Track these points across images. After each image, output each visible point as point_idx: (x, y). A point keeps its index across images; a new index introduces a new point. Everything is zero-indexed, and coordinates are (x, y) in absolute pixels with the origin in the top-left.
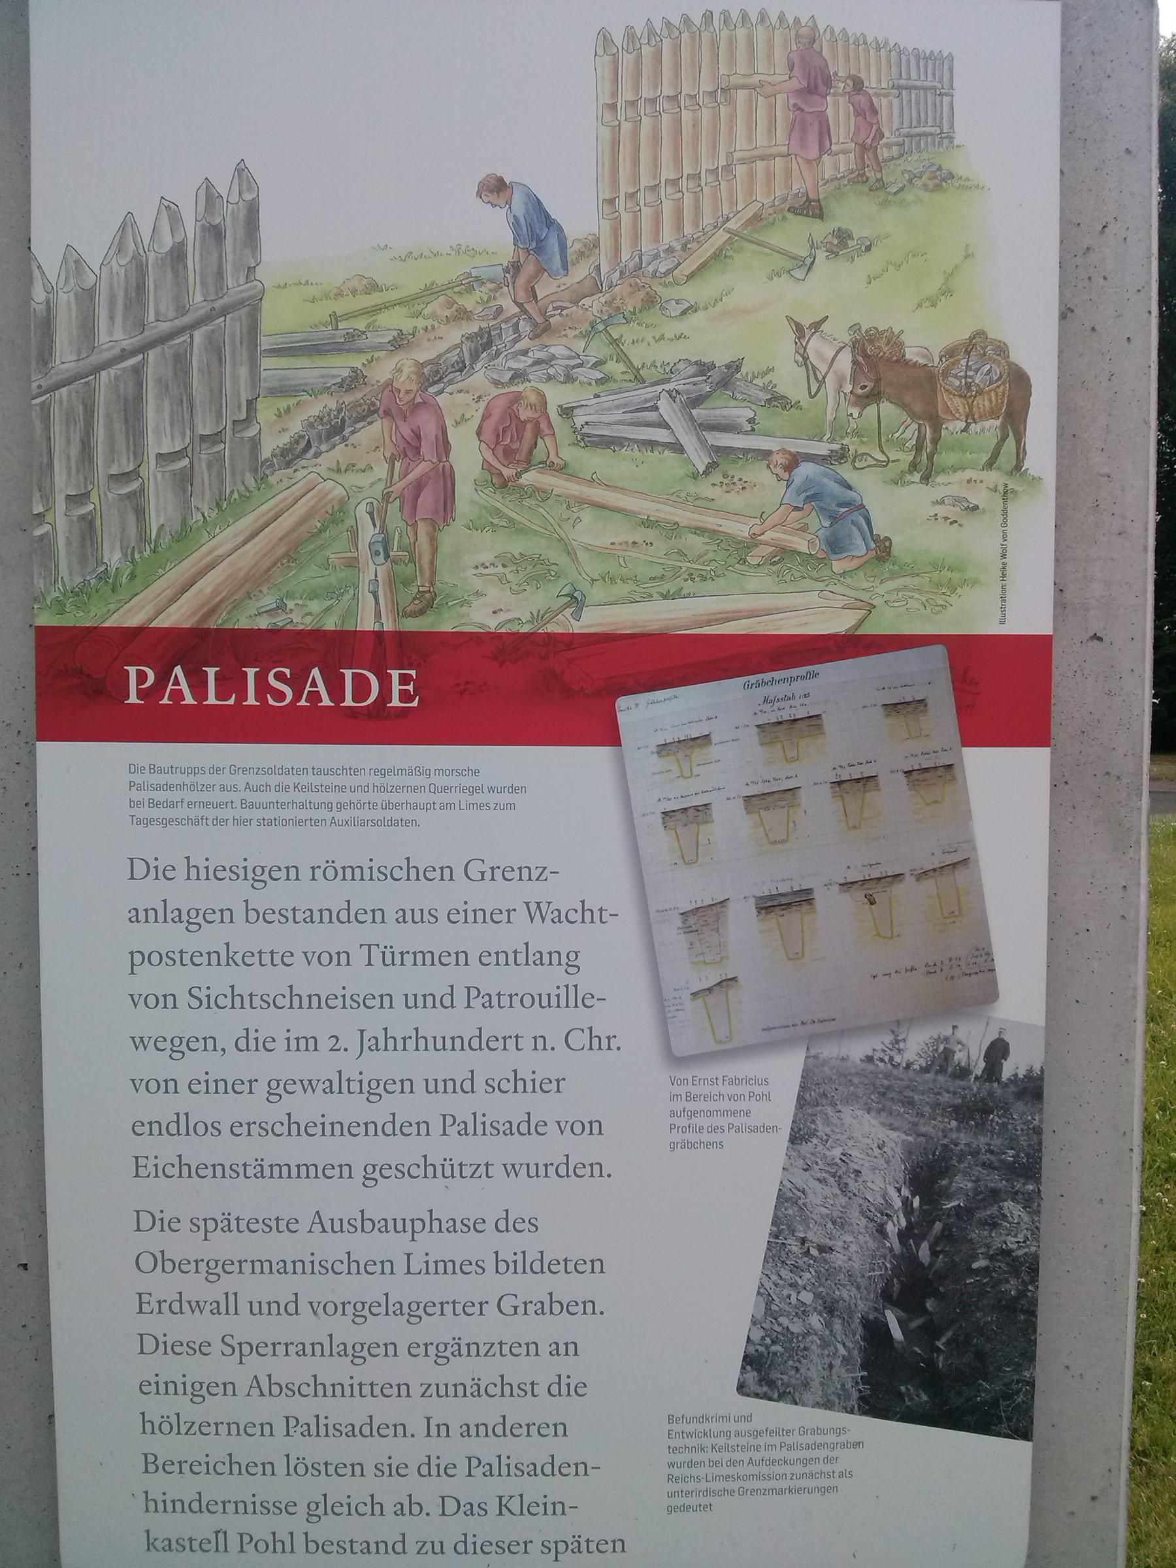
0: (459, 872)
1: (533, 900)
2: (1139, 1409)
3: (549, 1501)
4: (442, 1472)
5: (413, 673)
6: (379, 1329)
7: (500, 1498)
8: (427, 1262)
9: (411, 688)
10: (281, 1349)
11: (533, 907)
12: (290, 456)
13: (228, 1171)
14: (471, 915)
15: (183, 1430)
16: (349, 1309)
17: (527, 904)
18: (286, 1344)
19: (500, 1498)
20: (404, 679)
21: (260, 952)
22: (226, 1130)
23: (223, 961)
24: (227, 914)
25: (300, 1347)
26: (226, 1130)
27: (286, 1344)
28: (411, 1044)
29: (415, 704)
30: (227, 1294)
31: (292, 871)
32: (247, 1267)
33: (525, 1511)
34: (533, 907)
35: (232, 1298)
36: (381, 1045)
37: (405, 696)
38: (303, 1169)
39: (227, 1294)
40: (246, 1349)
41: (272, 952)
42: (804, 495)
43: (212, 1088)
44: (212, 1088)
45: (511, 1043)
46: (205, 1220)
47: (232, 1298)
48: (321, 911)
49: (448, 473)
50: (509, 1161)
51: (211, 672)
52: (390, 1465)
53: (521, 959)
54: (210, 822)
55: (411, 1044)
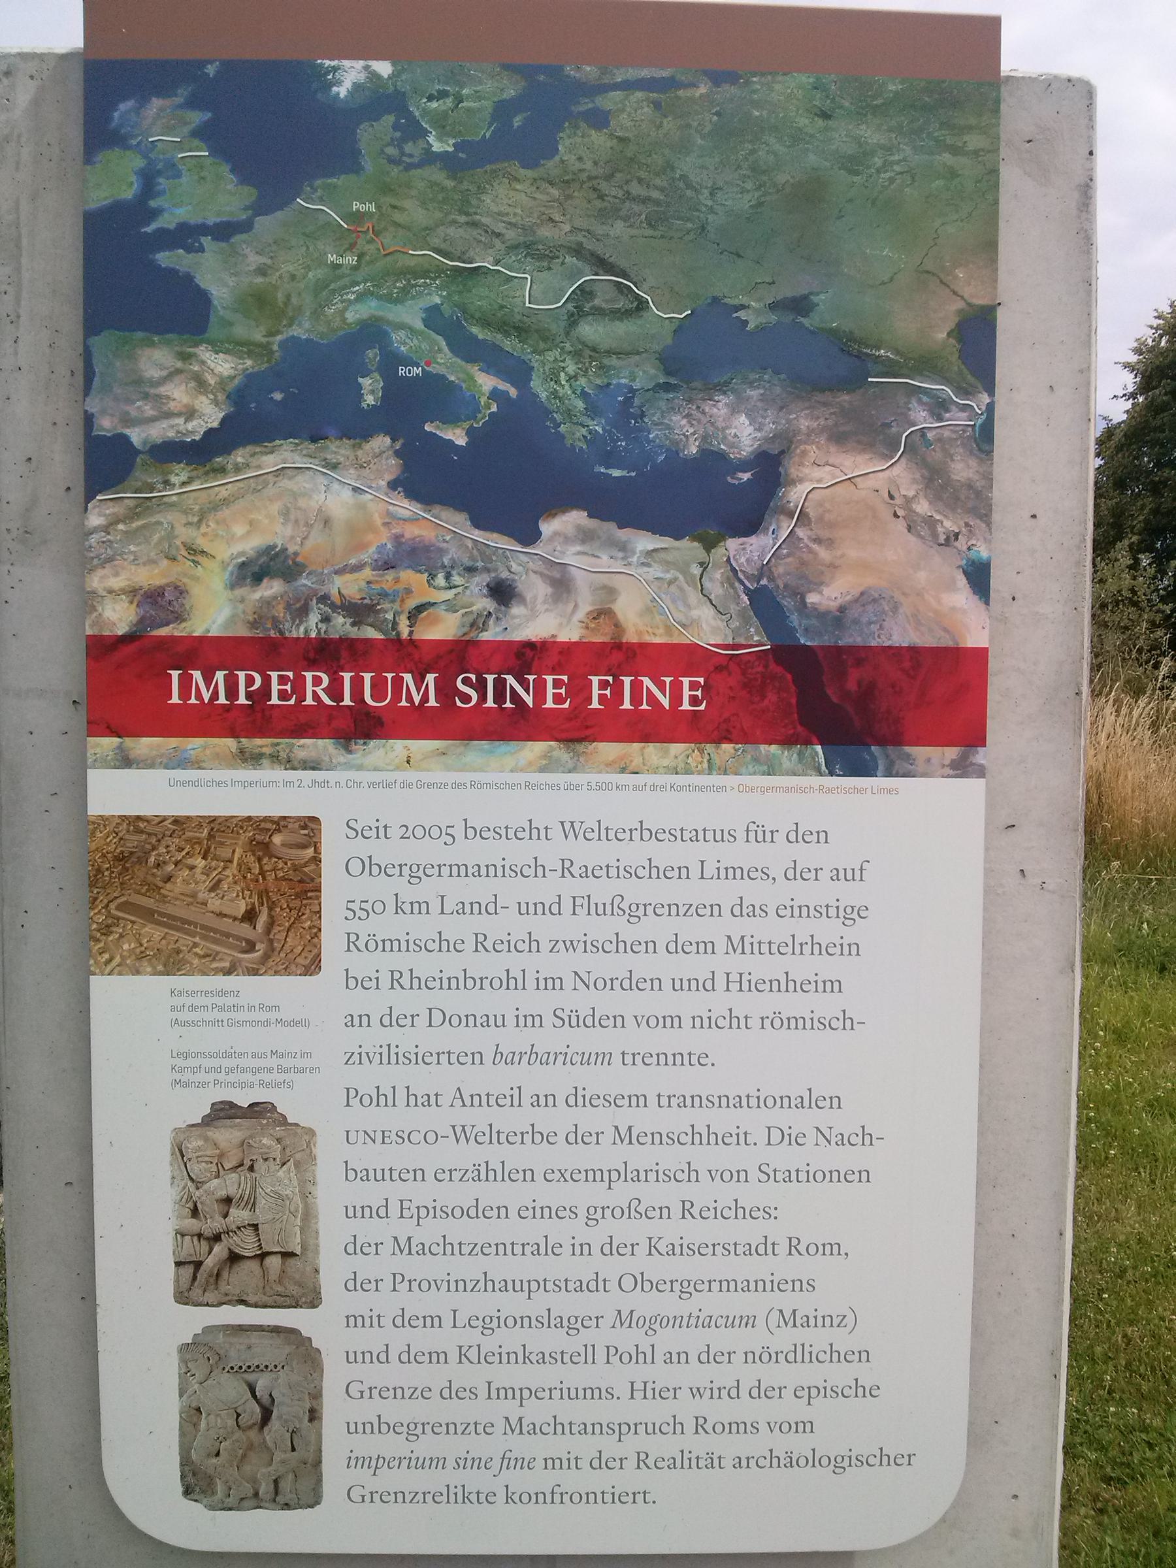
7: (460, 1347)
14: (505, 1357)
19: (460, 1347)
21: (608, 866)
22: (772, 911)
23: (521, 1359)
26: (772, 911)
30: (586, 1346)
31: (684, 871)
33: (482, 1360)
35: (590, 1349)
38: (589, 1392)
39: (586, 1346)
41: (770, 943)
43: (446, 985)
44: (446, 985)
45: (640, 1498)
47: (590, 1349)
49: (588, 732)
54: (225, 1023)
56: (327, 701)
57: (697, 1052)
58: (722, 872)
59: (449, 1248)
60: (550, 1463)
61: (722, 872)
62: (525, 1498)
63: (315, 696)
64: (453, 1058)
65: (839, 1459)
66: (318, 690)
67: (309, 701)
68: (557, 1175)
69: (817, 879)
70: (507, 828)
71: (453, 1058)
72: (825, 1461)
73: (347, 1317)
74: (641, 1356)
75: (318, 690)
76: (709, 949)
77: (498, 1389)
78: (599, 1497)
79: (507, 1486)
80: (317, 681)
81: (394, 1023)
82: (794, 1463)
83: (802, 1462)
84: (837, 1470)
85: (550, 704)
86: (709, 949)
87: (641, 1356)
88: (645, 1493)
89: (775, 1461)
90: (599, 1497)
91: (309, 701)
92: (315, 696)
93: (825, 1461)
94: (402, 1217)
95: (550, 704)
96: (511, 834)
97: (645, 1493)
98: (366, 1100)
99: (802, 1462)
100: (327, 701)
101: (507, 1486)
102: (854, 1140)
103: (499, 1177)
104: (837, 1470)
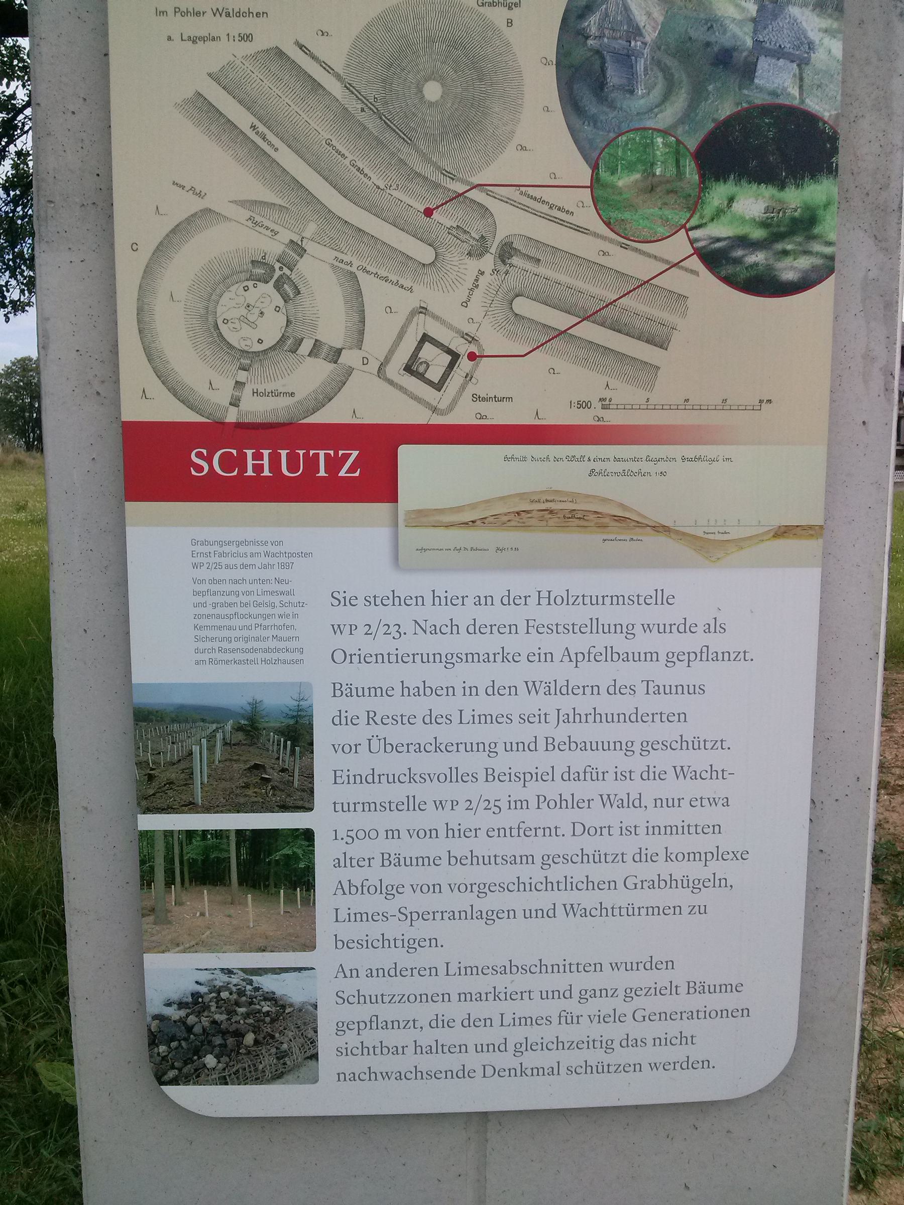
0: (620, 885)
1: (568, 902)
2: (309, 776)
3: (542, 652)
4: (649, 859)
10: (438, 916)
15: (571, 601)
16: (475, 888)
18: (442, 912)
25: (451, 913)
27: (442, 912)
28: (591, 718)
36: (571, 719)
40: (415, 916)
42: (593, 108)
43: (543, 659)
44: (543, 659)
48: (486, 597)
51: (322, 473)
53: (562, 886)
55: (591, 718)
58: (477, 718)
61: (477, 718)
62: (680, 857)
64: (664, 718)
68: (732, 855)
69: (434, 919)
71: (664, 718)
74: (564, 803)
76: (525, 806)
77: (700, 860)
79: (666, 848)
81: (570, 692)
86: (525, 806)
87: (564, 803)
88: (609, 827)
94: (335, 783)
96: (378, 601)
97: (609, 827)
101: (666, 848)
103: (570, 805)
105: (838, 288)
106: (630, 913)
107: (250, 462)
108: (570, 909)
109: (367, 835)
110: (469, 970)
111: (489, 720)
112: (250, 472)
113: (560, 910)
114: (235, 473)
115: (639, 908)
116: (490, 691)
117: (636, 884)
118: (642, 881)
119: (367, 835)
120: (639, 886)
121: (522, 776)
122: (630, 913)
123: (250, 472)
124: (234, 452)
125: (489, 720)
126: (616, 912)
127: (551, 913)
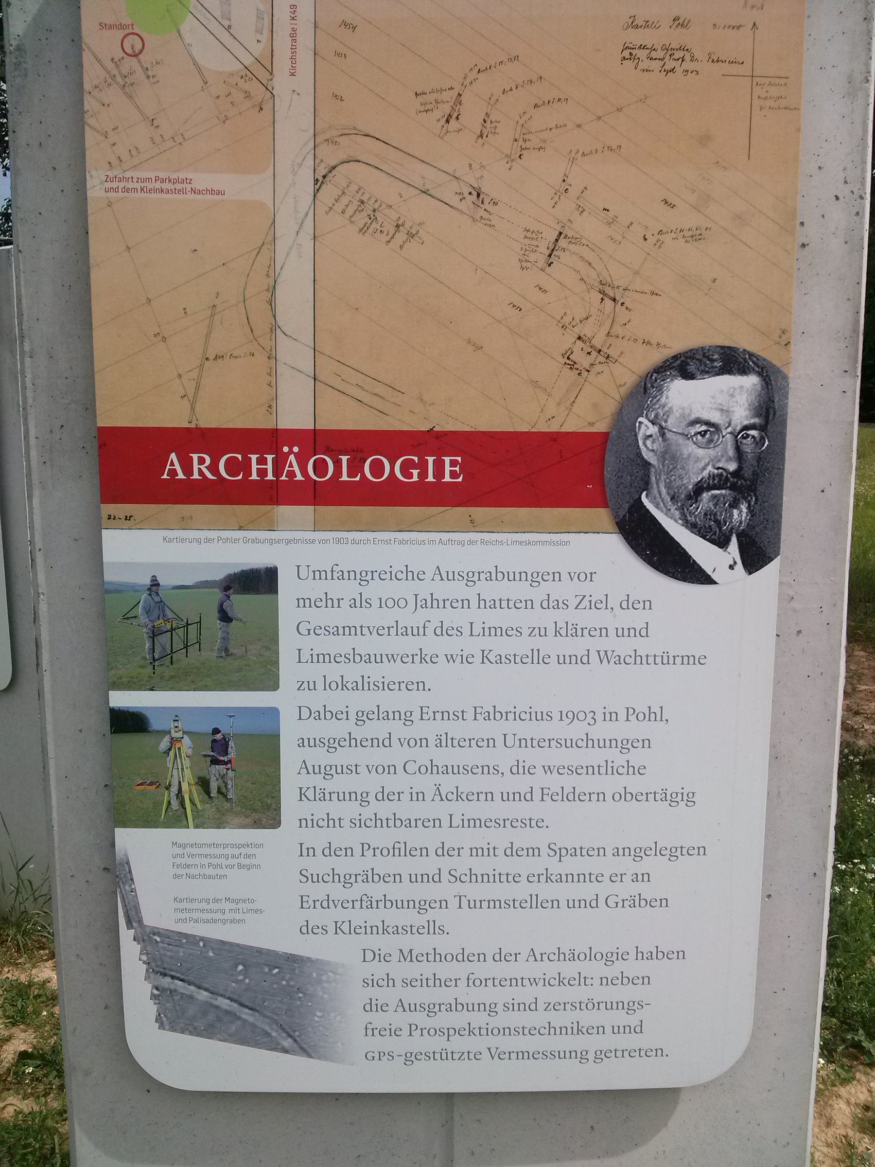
1: (602, 649)
5: (459, 459)
6: (344, 756)
8: (312, 655)
9: (457, 469)
11: (602, 654)
12: (708, 464)
13: (512, 1031)
17: (598, 652)
20: (453, 463)
24: (555, 903)
29: (460, 479)
32: (514, 1056)
34: (602, 654)
37: (453, 474)
41: (508, 600)
46: (448, 1029)
50: (546, 764)
52: (360, 820)
56: (209, 476)
57: (535, 817)
58: (487, 631)
59: (331, 822)
60: (475, 851)
63: (201, 472)
65: (609, 955)
66: (202, 467)
67: (196, 476)
70: (515, 655)
72: (599, 956)
73: (300, 820)
74: (653, 716)
75: (202, 467)
78: (596, 769)
80: (202, 461)
82: (576, 957)
83: (582, 957)
84: (608, 963)
85: (447, 478)
87: (653, 716)
89: (562, 956)
90: (596, 769)
91: (196, 476)
92: (201, 472)
93: (599, 956)
95: (447, 478)
98: (641, 717)
99: (582, 957)
100: (209, 476)
102: (628, 660)
104: (608, 963)
105: (782, 564)
106: (665, 661)
107: (254, 467)
108: (604, 656)
109: (396, 603)
110: (472, 822)
111: (499, 633)
112: (254, 476)
113: (594, 656)
114: (240, 477)
115: (674, 657)
116: (440, 852)
117: (617, 903)
118: (623, 901)
119: (396, 603)
120: (620, 905)
121: (446, 1032)
122: (665, 661)
123: (254, 476)
124: (239, 457)
125: (499, 633)
126: (651, 660)
127: (583, 660)
